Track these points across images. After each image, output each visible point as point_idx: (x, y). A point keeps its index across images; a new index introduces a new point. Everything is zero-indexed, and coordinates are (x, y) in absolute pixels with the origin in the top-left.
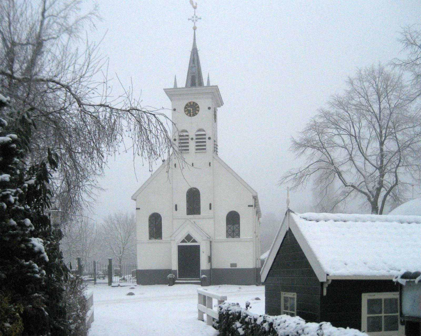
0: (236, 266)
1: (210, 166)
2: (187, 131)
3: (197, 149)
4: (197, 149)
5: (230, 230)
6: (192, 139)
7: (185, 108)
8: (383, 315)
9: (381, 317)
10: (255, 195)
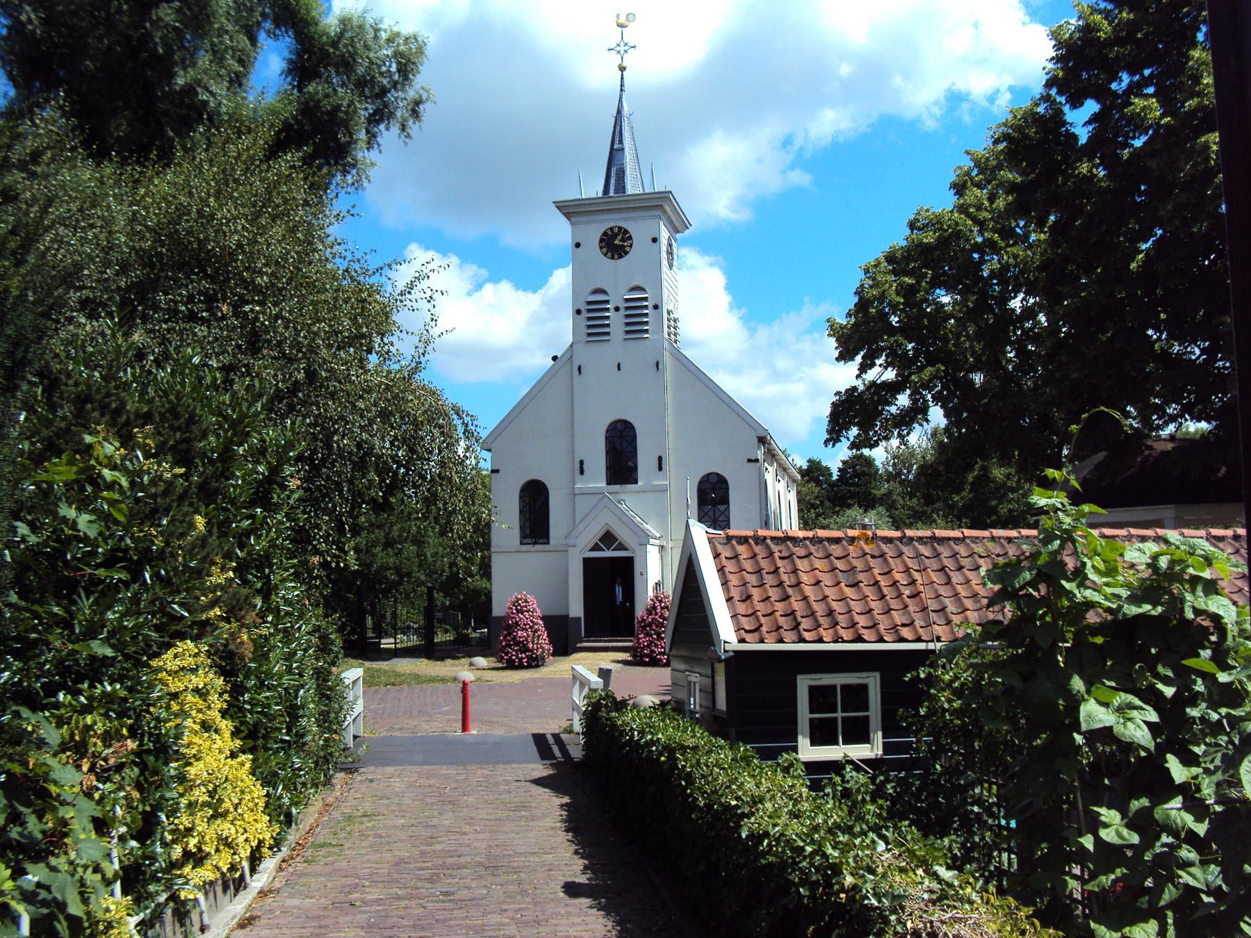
2: (603, 292)
3: (628, 332)
4: (628, 332)
8: (839, 715)
9: (836, 719)
10: (762, 434)
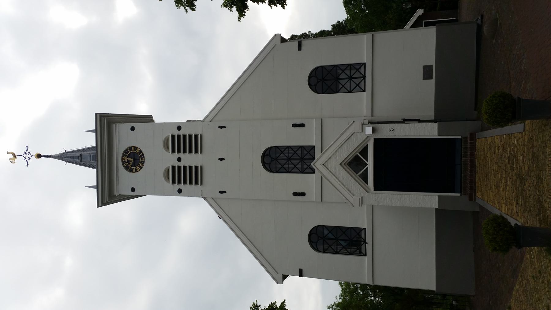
0: (431, 66)
1: (224, 127)
5: (347, 86)
6: (179, 160)
7: (131, 171)
